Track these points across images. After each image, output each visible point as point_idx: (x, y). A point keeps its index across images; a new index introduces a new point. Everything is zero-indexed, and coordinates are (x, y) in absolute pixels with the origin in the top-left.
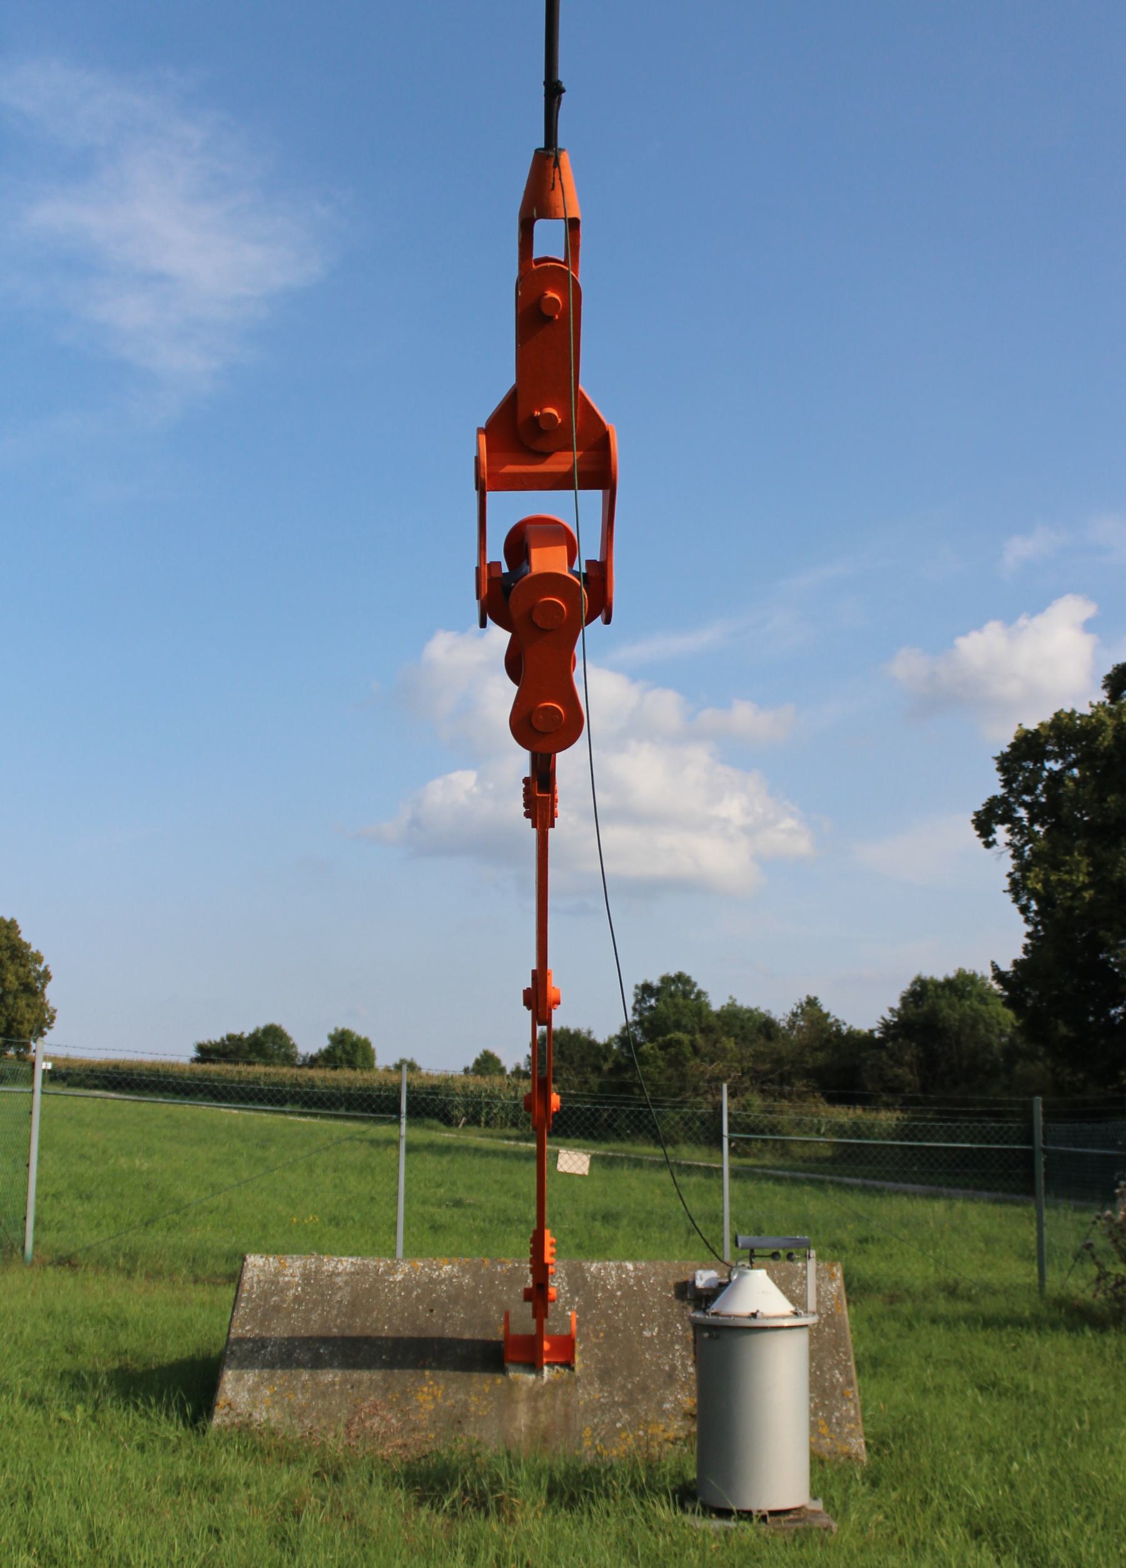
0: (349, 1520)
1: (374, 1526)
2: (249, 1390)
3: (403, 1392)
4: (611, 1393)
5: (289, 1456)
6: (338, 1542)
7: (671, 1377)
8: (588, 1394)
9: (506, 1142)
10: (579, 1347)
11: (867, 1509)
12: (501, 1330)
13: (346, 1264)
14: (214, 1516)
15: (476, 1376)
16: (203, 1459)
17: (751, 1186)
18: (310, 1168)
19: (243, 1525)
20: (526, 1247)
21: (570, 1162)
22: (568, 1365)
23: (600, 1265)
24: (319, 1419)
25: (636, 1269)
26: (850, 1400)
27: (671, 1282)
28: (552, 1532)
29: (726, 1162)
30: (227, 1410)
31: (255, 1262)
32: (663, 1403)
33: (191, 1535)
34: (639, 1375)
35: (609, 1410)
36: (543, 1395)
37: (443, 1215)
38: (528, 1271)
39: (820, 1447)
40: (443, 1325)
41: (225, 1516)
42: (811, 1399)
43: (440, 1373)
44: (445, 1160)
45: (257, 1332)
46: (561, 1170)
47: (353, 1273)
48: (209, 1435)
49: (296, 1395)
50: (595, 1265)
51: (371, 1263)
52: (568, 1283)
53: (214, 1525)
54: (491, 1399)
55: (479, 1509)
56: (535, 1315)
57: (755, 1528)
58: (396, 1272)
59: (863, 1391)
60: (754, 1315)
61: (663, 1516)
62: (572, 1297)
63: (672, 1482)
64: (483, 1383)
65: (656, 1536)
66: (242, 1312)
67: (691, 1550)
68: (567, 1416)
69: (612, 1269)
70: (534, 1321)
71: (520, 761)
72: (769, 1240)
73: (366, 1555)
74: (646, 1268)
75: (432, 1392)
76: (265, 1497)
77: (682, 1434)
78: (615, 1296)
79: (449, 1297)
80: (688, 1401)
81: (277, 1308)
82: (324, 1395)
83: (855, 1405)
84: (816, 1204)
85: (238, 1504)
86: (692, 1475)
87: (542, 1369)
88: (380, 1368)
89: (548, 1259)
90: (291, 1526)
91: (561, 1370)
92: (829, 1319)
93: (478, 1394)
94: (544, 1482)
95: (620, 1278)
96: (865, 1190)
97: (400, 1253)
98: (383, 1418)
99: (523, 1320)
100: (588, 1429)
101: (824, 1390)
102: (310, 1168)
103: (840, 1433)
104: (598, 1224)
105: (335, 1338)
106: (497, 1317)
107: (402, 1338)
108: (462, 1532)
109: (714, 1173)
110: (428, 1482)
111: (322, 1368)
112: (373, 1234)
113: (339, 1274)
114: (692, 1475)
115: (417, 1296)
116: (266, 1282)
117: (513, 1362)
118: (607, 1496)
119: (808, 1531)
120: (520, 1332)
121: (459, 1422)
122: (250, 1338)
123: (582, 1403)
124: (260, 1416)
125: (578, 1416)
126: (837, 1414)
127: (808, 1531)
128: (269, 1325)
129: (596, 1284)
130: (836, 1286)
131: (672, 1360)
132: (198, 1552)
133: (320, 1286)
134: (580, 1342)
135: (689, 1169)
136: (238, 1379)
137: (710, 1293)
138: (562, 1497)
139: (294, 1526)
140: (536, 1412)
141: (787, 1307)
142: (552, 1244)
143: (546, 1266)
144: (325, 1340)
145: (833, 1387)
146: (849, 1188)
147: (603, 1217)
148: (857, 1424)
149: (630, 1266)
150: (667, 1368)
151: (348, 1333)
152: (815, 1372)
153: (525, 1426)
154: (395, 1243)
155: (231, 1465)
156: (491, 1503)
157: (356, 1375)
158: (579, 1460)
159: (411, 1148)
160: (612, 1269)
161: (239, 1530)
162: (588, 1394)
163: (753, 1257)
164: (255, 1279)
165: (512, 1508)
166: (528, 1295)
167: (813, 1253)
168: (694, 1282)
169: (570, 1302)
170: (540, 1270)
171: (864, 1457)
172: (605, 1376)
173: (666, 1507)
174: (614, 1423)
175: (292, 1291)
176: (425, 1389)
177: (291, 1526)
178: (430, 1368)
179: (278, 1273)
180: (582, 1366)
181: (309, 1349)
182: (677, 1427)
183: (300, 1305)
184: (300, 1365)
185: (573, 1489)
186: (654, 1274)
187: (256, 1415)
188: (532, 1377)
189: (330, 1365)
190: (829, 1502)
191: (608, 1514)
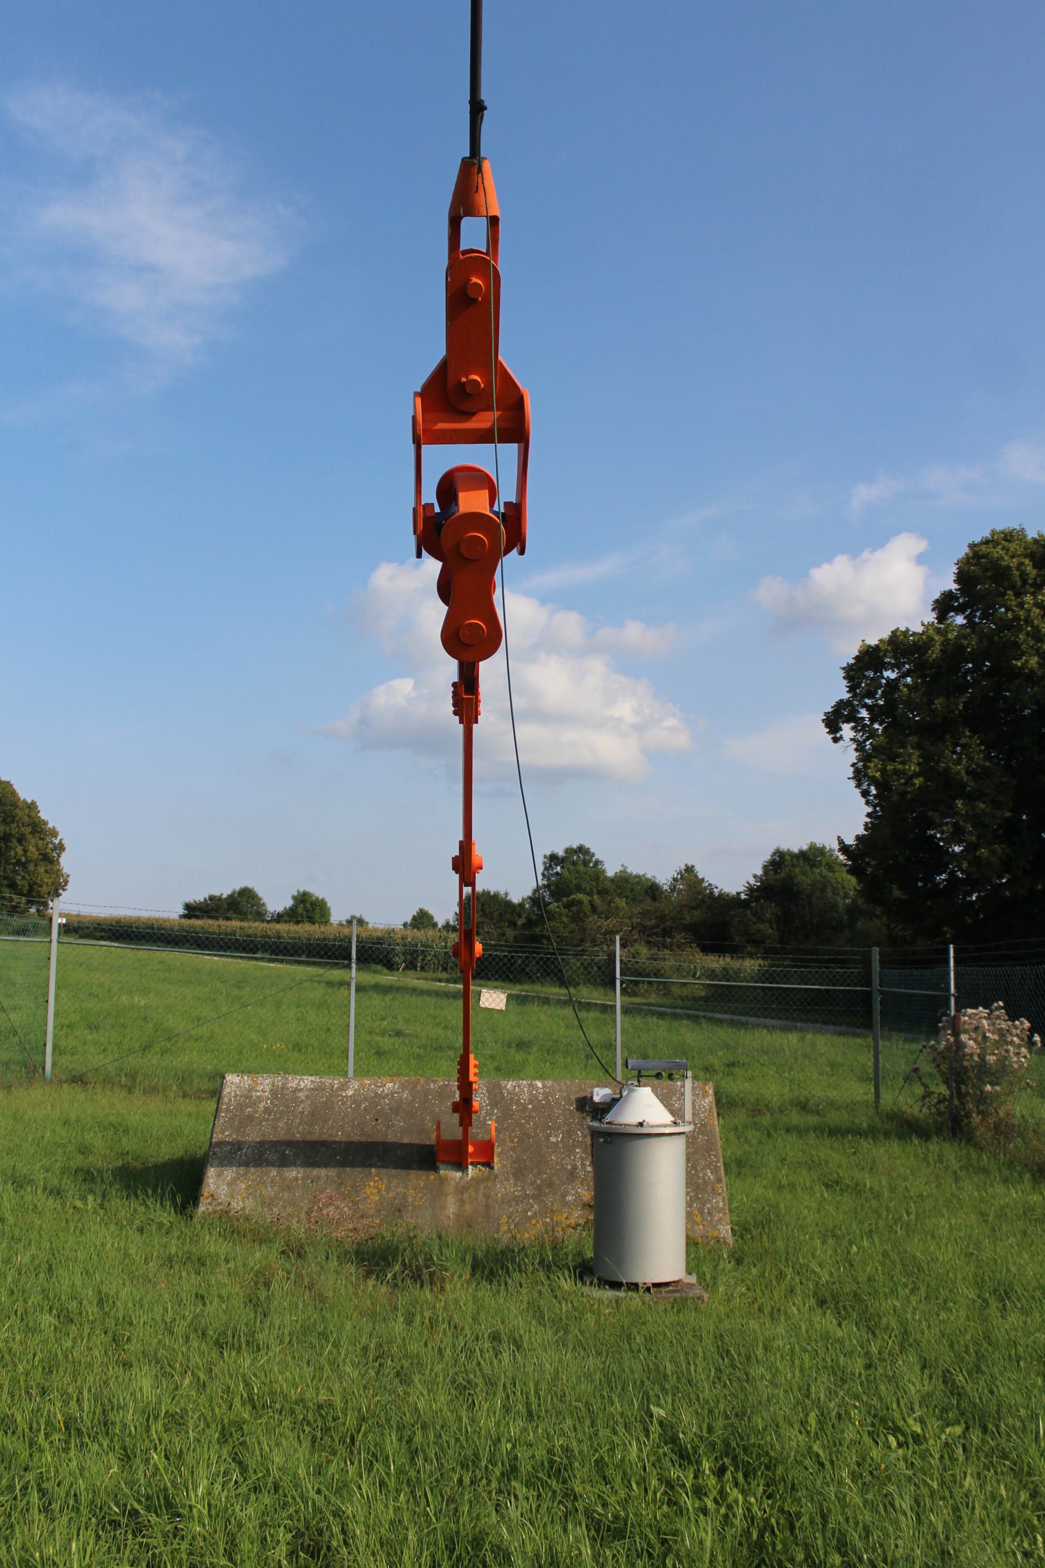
0: (310, 1290)
1: (330, 1294)
3: (354, 1186)
4: (523, 1188)
5: (260, 1238)
6: (301, 1306)
7: (572, 1174)
8: (505, 1188)
10: (497, 1150)
11: (733, 1283)
12: (434, 1136)
13: (307, 1082)
15: (413, 1174)
17: (638, 1020)
18: (278, 1005)
19: (223, 1292)
21: (491, 1000)
22: (489, 1164)
24: (285, 1207)
25: (544, 1086)
27: (573, 1097)
28: (475, 1300)
33: (182, 1300)
36: (468, 1189)
37: (386, 1043)
42: (687, 1193)
47: (312, 1089)
48: (195, 1220)
49: (266, 1187)
51: (327, 1081)
52: (489, 1098)
53: (200, 1292)
55: (415, 1281)
56: (461, 1125)
58: (348, 1088)
59: (729, 1186)
60: (641, 1124)
63: (573, 1260)
64: (419, 1179)
71: (449, 669)
72: (654, 1063)
75: (377, 1187)
77: (582, 1221)
79: (391, 1109)
80: (587, 1194)
81: (250, 1117)
82: (289, 1188)
85: (220, 1275)
86: (590, 1254)
87: (467, 1168)
88: (334, 1167)
89: (472, 1078)
90: (263, 1294)
92: (702, 1128)
93: (414, 1188)
94: (469, 1259)
96: (732, 1024)
97: (351, 1074)
98: (337, 1208)
101: (698, 1186)
104: (513, 1051)
106: (430, 1125)
107: (352, 1143)
110: (374, 1258)
112: (329, 1056)
113: (301, 1090)
114: (590, 1254)
117: (443, 1162)
118: (520, 1271)
120: (449, 1138)
124: (237, 1205)
126: (708, 1205)
127: (684, 1300)
129: (512, 1099)
130: (709, 1100)
132: (187, 1314)
134: (498, 1147)
135: (588, 1006)
136: (219, 1175)
138: (483, 1272)
140: (462, 1202)
141: (668, 1118)
142: (475, 1066)
144: (289, 1144)
148: (725, 1214)
149: (539, 1084)
151: (308, 1138)
154: (347, 1065)
155: (212, 1244)
156: (426, 1277)
157: (315, 1172)
159: (359, 989)
161: (220, 1296)
162: (505, 1188)
163: (639, 1077)
165: (443, 1280)
166: (456, 1107)
167: (690, 1074)
168: (592, 1097)
169: (489, 1114)
171: (730, 1240)
172: (519, 1173)
176: (372, 1184)
178: (375, 1166)
181: (277, 1151)
182: (578, 1216)
184: (270, 1164)
185: (492, 1265)
187: (234, 1204)
188: (459, 1174)
189: (295, 1165)
190: (701, 1277)
191: (521, 1286)
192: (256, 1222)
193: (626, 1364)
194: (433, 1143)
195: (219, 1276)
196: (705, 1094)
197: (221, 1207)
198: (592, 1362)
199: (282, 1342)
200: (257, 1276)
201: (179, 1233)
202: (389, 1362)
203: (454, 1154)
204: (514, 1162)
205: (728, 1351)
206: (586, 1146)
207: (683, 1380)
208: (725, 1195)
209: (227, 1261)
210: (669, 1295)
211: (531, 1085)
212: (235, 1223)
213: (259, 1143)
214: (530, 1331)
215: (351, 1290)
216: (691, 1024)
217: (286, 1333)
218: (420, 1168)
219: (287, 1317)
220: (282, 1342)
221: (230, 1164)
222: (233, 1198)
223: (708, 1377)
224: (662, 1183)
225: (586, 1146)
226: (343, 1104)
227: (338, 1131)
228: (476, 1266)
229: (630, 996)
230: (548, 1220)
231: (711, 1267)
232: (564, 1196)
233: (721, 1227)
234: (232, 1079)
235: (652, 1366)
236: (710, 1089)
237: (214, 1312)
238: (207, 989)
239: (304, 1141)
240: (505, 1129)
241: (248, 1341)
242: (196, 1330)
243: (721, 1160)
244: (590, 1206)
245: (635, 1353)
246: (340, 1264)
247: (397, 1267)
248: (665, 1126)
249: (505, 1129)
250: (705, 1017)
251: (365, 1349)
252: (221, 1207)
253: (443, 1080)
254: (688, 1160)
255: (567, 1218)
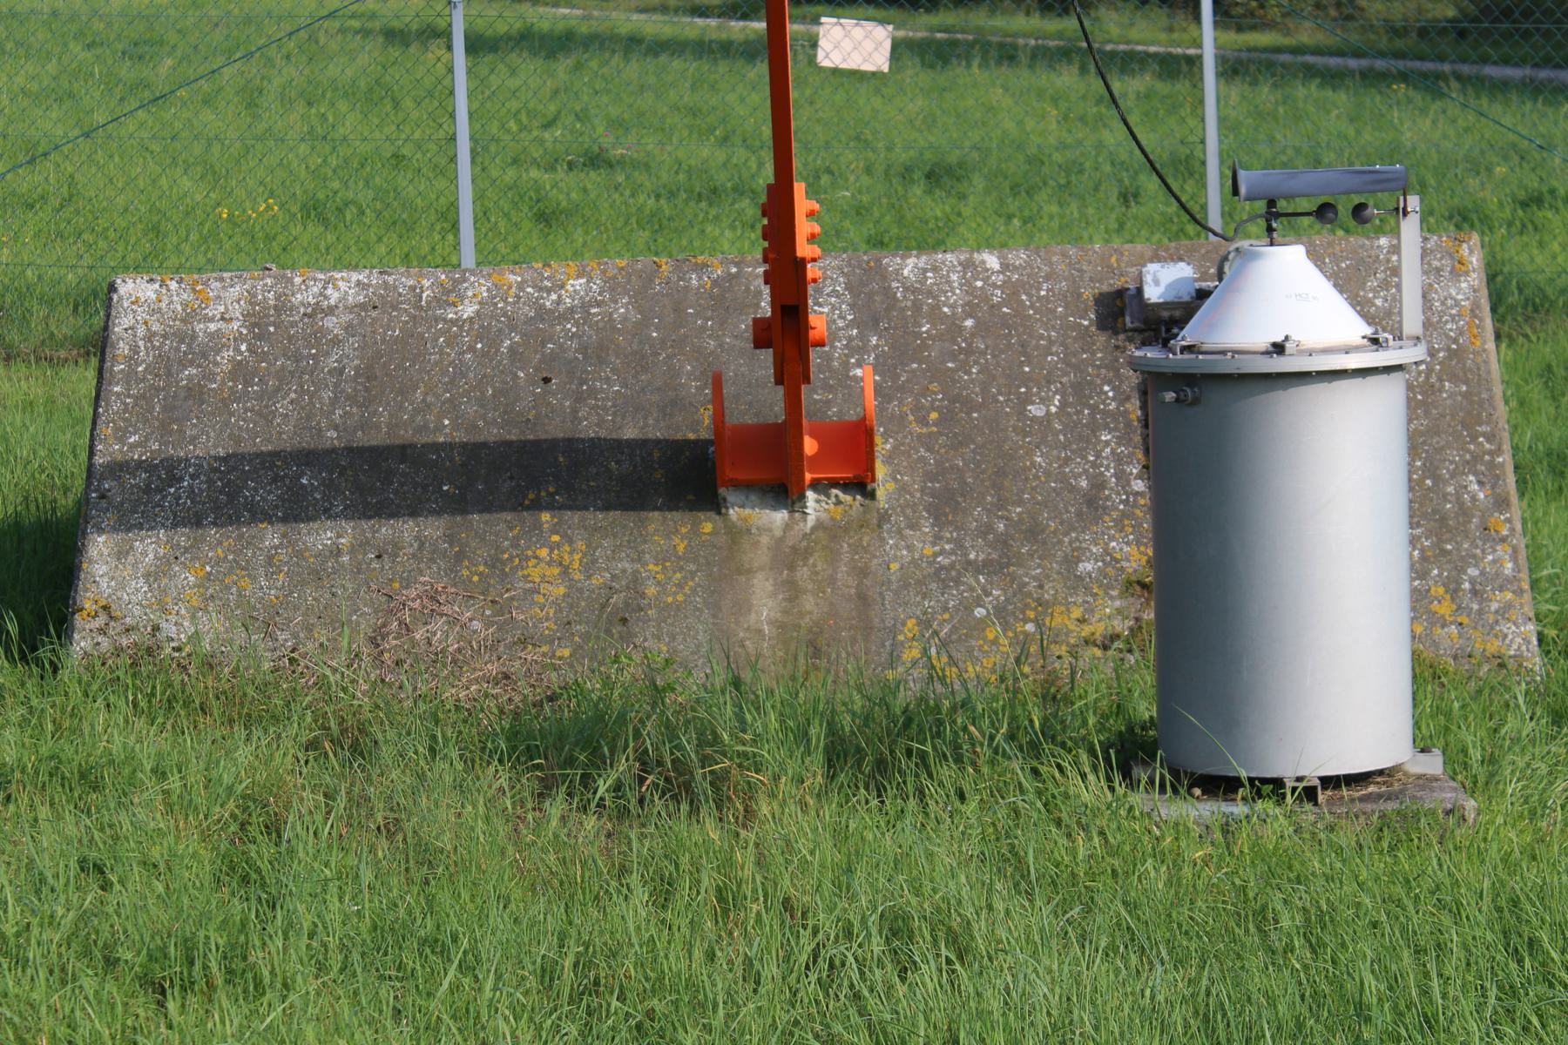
0: (391, 836)
1: (446, 841)
2: (147, 575)
3: (494, 563)
4: (958, 543)
5: (247, 709)
6: (367, 876)
7: (1093, 503)
8: (908, 546)
9: (699, 21)
10: (883, 446)
11: (1544, 769)
12: (706, 417)
13: (345, 287)
14: (92, 840)
15: (655, 520)
16: (58, 726)
17: (1265, 94)
18: (251, 98)
19: (156, 854)
20: (755, 247)
21: (847, 45)
22: (861, 485)
23: (923, 261)
24: (309, 629)
25: (1005, 267)
26: (1503, 540)
27: (1088, 294)
28: (840, 835)
29: (1209, 38)
30: (101, 620)
31: (136, 292)
32: (1079, 560)
33: (43, 880)
34: (1020, 502)
35: (958, 582)
36: (807, 554)
37: (563, 187)
38: (761, 281)
39: (1436, 644)
40: (575, 411)
41: (115, 838)
42: (1413, 541)
43: (572, 517)
44: (563, 65)
45: (156, 446)
46: (826, 63)
47: (362, 306)
48: (64, 674)
49: (254, 579)
50: (911, 261)
51: (403, 281)
52: (852, 306)
53: (93, 855)
54: (692, 567)
55: (676, 799)
56: (779, 380)
57: (1288, 816)
58: (462, 298)
59: (1532, 524)
60: (1279, 348)
61: (1086, 797)
62: (862, 336)
63: (1101, 728)
64: (671, 535)
65: (1069, 835)
66: (116, 406)
67: (1149, 863)
68: (863, 598)
69: (952, 269)
70: (781, 390)
72: (1309, 183)
73: (430, 900)
74: (1029, 264)
75: (559, 562)
76: (200, 799)
77: (1122, 626)
78: (961, 329)
79: (583, 349)
80: (1135, 556)
81: (195, 393)
82: (317, 576)
83: (1515, 550)
84: (1421, 126)
85: (146, 810)
86: (1145, 710)
87: (802, 497)
88: (437, 513)
89: (803, 249)
90: (262, 852)
91: (847, 498)
92: (1453, 361)
93: (661, 559)
94: (817, 731)
95: (969, 288)
96: (1534, 89)
97: (468, 257)
98: (453, 621)
99: (755, 391)
100: (911, 623)
101: (1443, 520)
102: (251, 98)
103: (1480, 612)
104: (918, 190)
105: (334, 450)
106: (693, 387)
107: (485, 445)
108: (641, 844)
109: (1182, 67)
110: (560, 748)
111: (310, 519)
112: (409, 225)
113: (331, 310)
114: (1145, 710)
115: (511, 349)
116: (165, 336)
117: (736, 485)
118: (959, 759)
119: (1409, 819)
120: (749, 420)
121: (624, 621)
122: (140, 463)
123: (894, 566)
124: (176, 629)
125: (889, 596)
126: (1473, 572)
127: (1409, 819)
128: (181, 431)
129: (917, 306)
130: (1469, 287)
131: (1094, 465)
132: (60, 911)
133: (290, 338)
134: (886, 436)
135: (1131, 62)
136: (121, 554)
137: (1177, 314)
138: (859, 763)
139: (268, 850)
140: (792, 592)
141: (1354, 328)
142: (811, 214)
143: (801, 264)
144: (308, 458)
145: (1464, 512)
146: (1500, 88)
147: (928, 176)
148: (1519, 592)
149: (992, 261)
150: (1084, 484)
151: (362, 439)
152: (1421, 482)
153: (770, 622)
154: (456, 246)
155: (113, 733)
156: (702, 785)
157: (386, 530)
158: (893, 689)
159: (475, 45)
160: (952, 269)
161: (149, 865)
162: (908, 546)
163: (1275, 219)
164: (141, 331)
165: (750, 791)
166: (763, 335)
167: (1413, 202)
168: (1140, 291)
169: (858, 349)
170: (787, 275)
171: (1535, 661)
172: (944, 506)
173: (1091, 777)
174: (969, 610)
175: (227, 354)
176: (544, 553)
177: (262, 852)
178: (550, 507)
179: (190, 316)
180: (891, 486)
181: (275, 480)
182: (1112, 613)
183: (247, 383)
184: (259, 514)
185: (881, 750)
186: (1047, 278)
187: (168, 629)
188: (780, 516)
189: (328, 513)
190: (1456, 760)
191: (962, 797)
192: (234, 673)
193: (1256, 982)
194: (705, 434)
195: (141, 814)
196: (1459, 269)
197: (134, 637)
198: (1163, 982)
199: (321, 968)
200: (245, 809)
201: (22, 711)
202: (615, 1003)
203: (767, 462)
204: (930, 476)
205: (1532, 943)
206: (1128, 424)
207: (1411, 1018)
208: (1521, 542)
209: (160, 773)
210: (1369, 807)
211: (967, 265)
212: (177, 678)
213: (225, 459)
214: (990, 907)
215: (503, 829)
216: (1417, 97)
217: (333, 942)
218: (672, 504)
219: (334, 905)
220: (321, 968)
221: (147, 522)
222: (165, 611)
223: (1480, 1008)
224: (1342, 515)
225: (1128, 424)
226: (448, 343)
227: (442, 418)
228: (838, 754)
229: (1240, 29)
230: (1030, 627)
231: (1482, 733)
232: (1071, 561)
233: (1508, 628)
234: (134, 290)
235: (1324, 987)
236: (1473, 256)
237: (135, 909)
238: (51, 68)
239: (350, 450)
240: (902, 389)
241: (230, 971)
242: (86, 953)
243: (1506, 447)
244: (1144, 586)
245: (1277, 956)
246: (470, 764)
247: (623, 766)
248: (1347, 350)
249: (902, 389)
250: (1459, 77)
251: (548, 973)
252: (134, 637)
253: (725, 262)
254: (1413, 450)
255: (1082, 621)
